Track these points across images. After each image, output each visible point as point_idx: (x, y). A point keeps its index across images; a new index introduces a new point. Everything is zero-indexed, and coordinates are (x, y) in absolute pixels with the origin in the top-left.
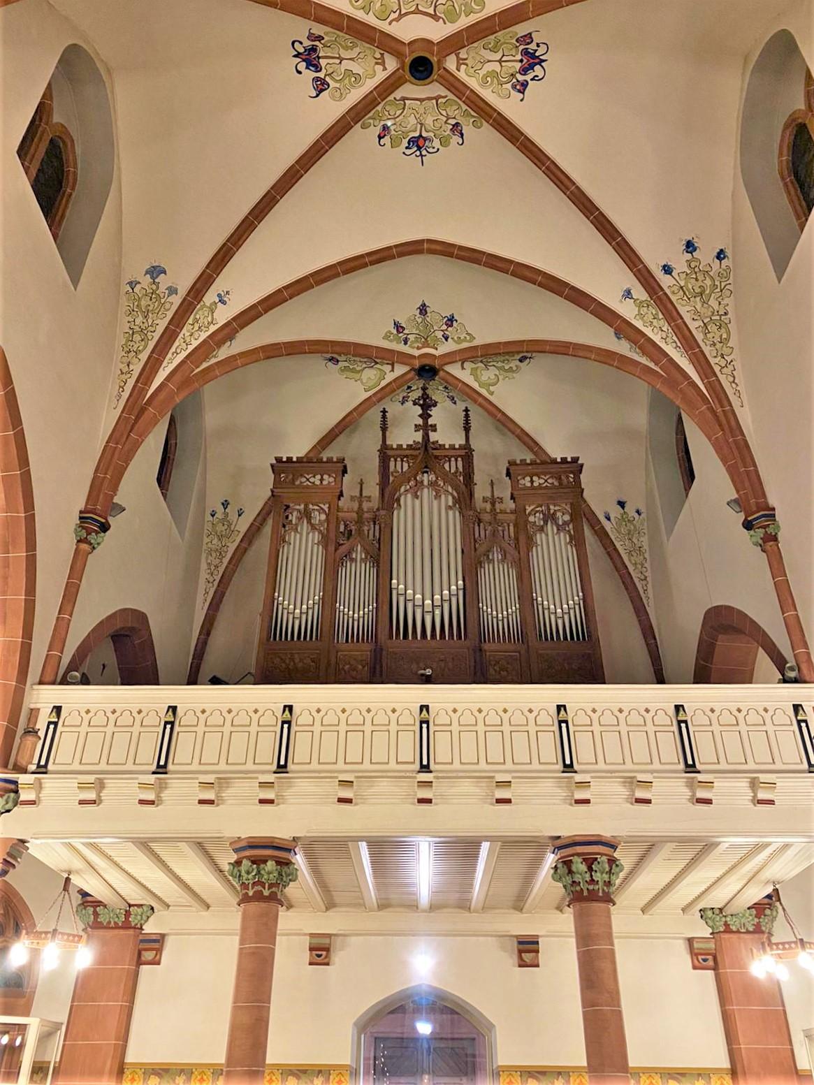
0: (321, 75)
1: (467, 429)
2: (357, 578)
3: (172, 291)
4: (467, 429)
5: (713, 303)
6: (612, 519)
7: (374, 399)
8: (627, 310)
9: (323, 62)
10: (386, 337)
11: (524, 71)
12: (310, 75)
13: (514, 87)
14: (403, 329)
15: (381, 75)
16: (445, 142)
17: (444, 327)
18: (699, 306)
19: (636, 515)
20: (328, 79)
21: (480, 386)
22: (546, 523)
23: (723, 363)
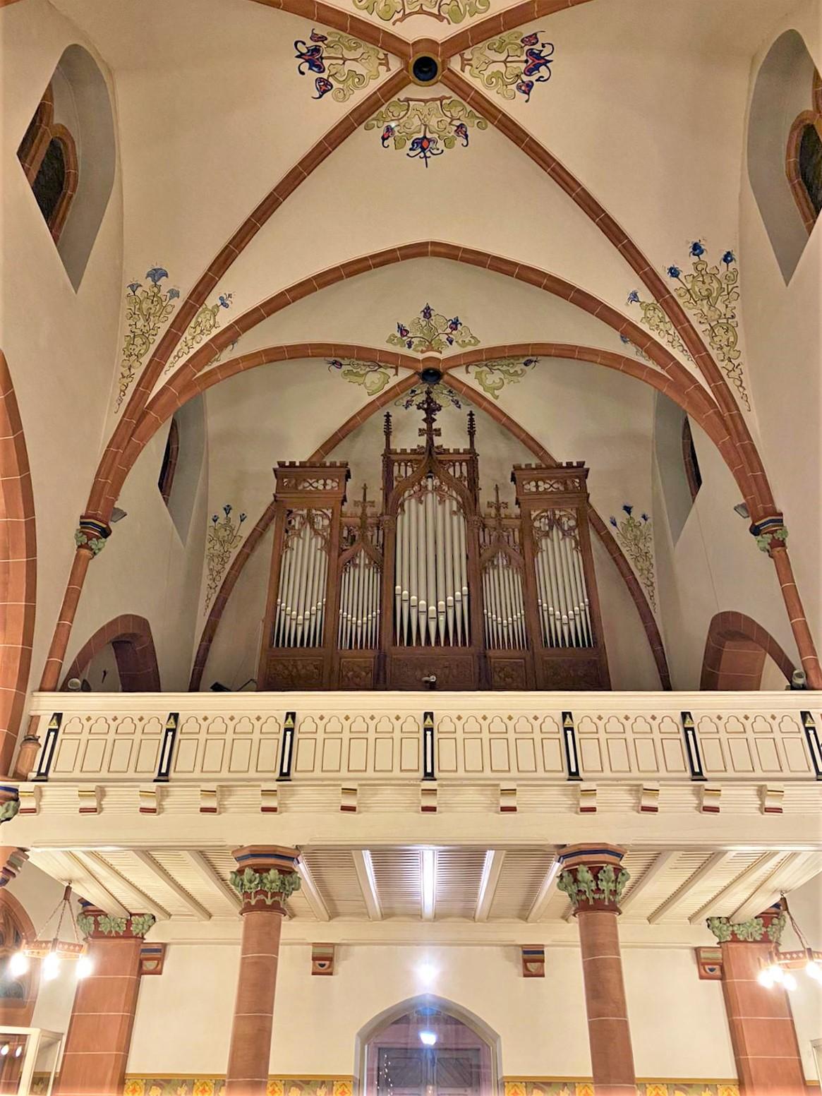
0: (324, 75)
1: (472, 433)
2: (361, 584)
3: (174, 294)
4: (472, 433)
5: (720, 306)
6: (618, 524)
7: (378, 403)
8: (633, 313)
9: (326, 63)
10: (390, 341)
11: (529, 72)
12: (313, 75)
13: (519, 88)
14: (407, 332)
15: (385, 76)
16: (449, 143)
17: (449, 330)
18: (705, 309)
19: (642, 521)
20: (331, 80)
21: (484, 390)
22: (551, 528)
23: (730, 367)
